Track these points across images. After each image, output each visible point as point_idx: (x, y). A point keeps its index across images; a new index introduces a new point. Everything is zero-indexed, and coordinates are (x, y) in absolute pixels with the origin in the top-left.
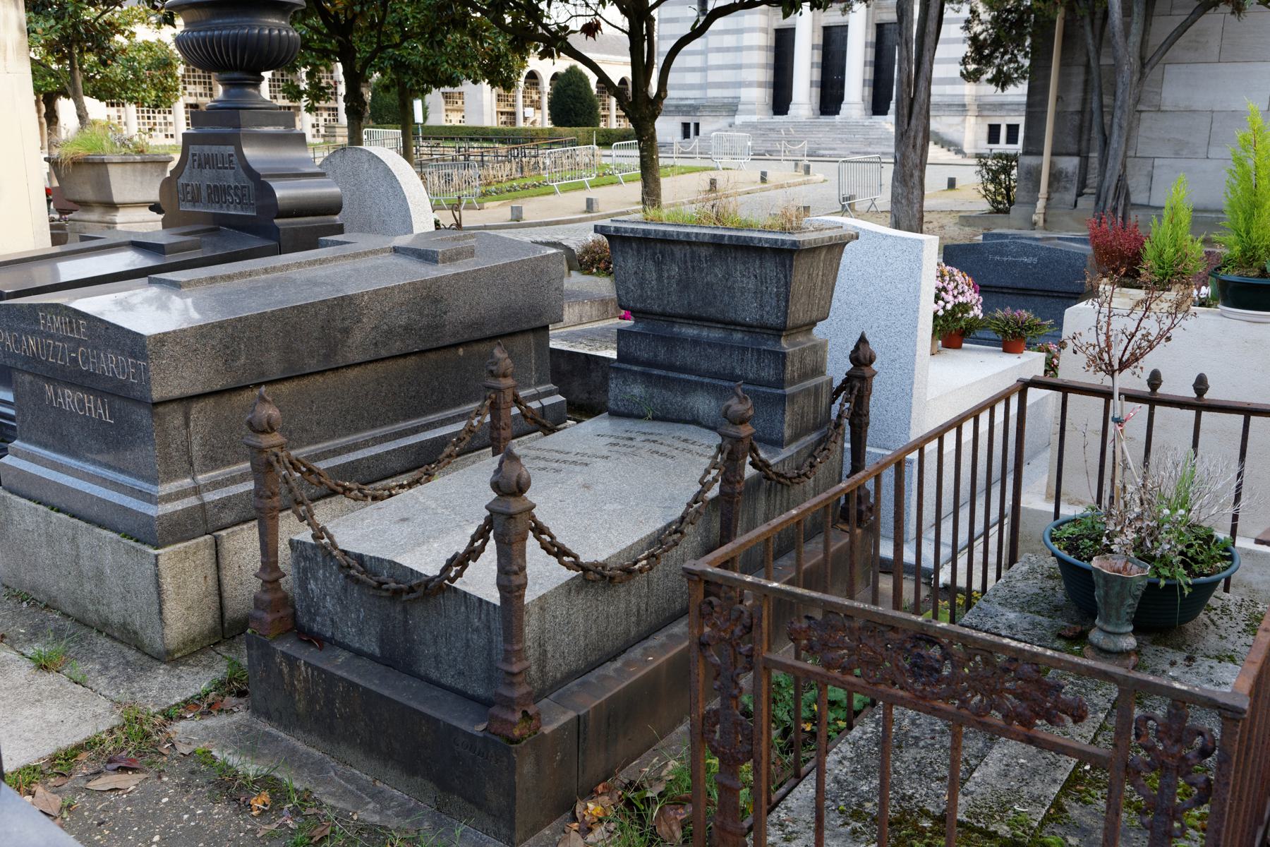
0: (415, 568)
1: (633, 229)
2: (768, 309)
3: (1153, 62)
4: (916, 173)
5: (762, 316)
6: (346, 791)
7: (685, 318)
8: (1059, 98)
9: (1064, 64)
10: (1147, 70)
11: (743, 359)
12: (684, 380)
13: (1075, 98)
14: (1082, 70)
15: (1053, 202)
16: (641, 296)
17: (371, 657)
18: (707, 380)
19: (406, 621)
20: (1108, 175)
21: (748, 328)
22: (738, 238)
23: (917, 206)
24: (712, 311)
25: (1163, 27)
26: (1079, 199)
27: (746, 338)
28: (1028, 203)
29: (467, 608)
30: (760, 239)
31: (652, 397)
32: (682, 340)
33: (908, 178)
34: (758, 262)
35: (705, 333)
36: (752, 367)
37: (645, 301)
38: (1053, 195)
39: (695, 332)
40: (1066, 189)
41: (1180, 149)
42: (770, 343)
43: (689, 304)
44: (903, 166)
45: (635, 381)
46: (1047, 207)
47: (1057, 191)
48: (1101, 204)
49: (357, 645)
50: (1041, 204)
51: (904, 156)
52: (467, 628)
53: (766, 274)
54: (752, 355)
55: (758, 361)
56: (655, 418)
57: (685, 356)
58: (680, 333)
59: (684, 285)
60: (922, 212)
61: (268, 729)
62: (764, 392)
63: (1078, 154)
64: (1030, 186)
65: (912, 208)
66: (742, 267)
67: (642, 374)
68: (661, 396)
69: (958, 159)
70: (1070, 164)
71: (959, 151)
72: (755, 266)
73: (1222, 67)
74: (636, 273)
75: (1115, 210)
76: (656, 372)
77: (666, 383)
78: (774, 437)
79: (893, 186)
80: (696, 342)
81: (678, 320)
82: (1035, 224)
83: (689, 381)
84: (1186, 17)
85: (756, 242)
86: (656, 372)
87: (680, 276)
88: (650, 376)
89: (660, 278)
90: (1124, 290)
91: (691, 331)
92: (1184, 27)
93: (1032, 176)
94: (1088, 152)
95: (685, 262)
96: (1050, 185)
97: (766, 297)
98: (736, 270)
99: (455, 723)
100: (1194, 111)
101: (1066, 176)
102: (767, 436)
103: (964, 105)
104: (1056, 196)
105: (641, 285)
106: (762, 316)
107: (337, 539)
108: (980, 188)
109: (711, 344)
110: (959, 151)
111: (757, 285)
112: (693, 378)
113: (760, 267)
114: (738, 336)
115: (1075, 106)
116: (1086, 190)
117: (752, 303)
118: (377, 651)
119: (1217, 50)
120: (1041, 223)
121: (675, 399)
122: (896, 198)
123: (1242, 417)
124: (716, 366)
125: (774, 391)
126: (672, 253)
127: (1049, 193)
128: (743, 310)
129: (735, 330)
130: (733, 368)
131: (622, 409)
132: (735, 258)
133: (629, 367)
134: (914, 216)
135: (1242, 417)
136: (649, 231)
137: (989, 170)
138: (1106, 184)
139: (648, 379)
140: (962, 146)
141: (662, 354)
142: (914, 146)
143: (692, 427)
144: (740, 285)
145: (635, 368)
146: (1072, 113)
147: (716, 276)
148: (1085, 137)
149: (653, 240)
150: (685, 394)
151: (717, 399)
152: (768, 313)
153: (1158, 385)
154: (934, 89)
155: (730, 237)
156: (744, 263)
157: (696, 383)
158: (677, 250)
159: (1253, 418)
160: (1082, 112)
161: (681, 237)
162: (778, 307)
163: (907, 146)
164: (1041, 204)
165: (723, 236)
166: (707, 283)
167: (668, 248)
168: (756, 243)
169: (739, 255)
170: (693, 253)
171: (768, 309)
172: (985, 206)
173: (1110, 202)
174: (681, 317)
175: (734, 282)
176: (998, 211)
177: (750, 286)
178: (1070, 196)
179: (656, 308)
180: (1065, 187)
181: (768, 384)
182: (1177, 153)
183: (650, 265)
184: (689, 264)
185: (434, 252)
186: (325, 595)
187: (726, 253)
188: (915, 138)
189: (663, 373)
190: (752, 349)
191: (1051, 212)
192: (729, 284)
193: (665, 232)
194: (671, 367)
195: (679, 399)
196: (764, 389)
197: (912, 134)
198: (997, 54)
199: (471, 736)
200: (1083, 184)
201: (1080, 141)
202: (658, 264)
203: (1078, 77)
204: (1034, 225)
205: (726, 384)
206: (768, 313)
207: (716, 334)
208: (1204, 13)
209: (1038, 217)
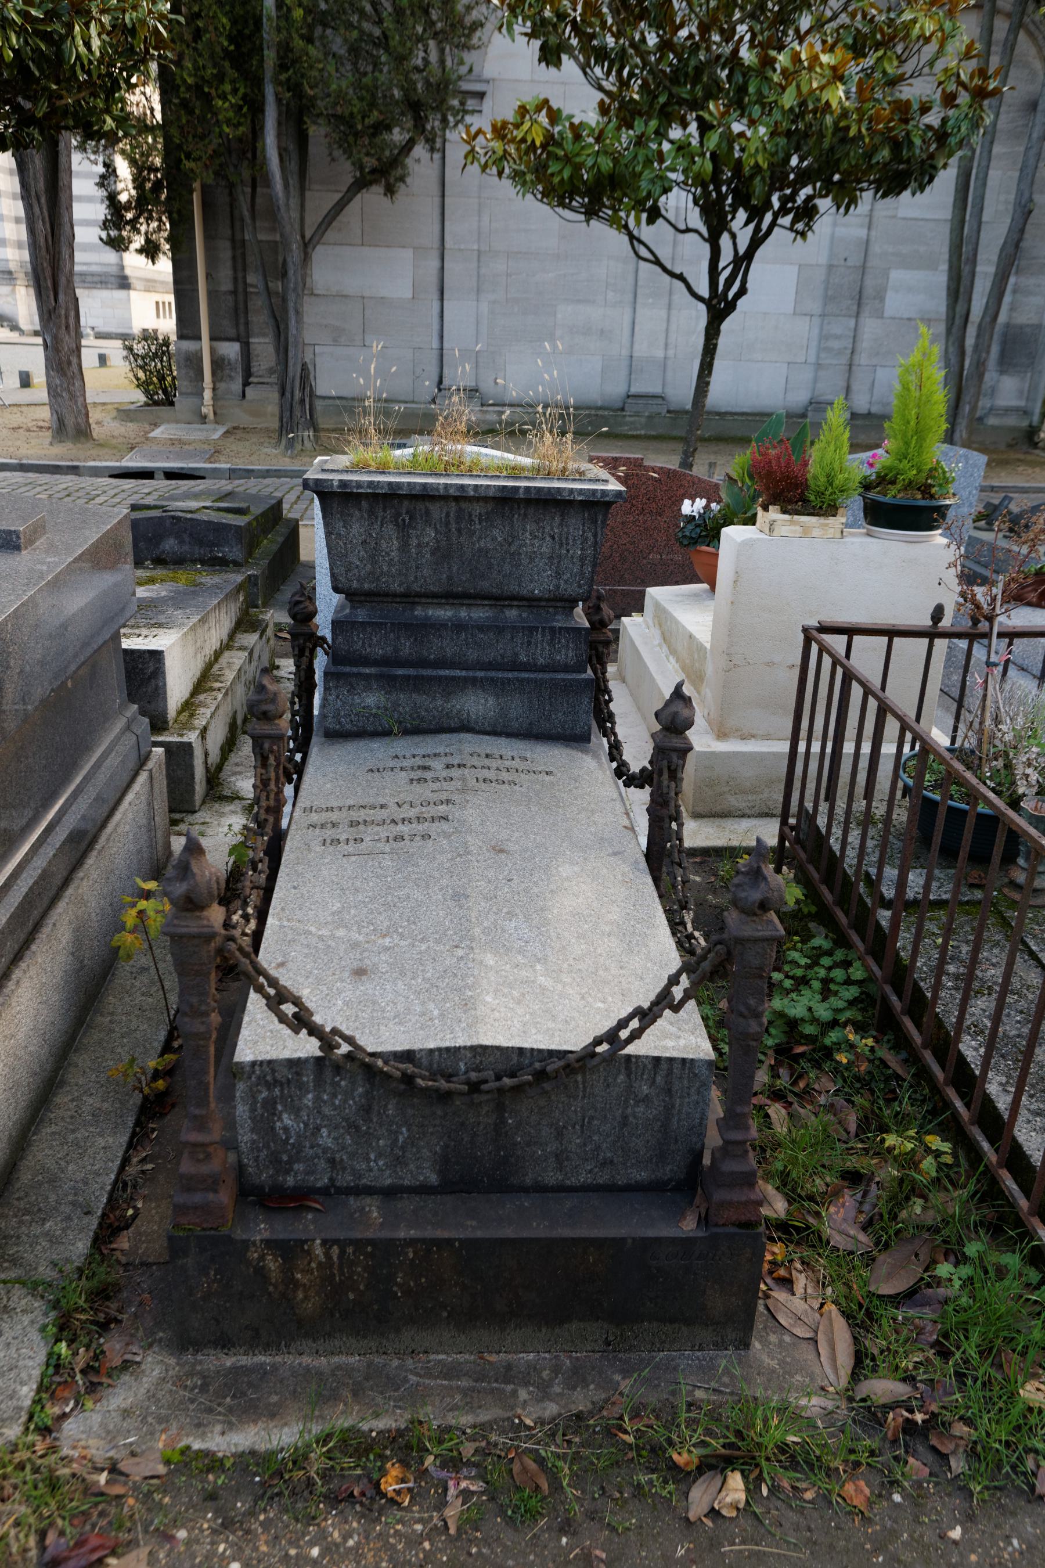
0: (526, 1045)
1: (371, 482)
2: (567, 576)
3: (314, 241)
4: (74, 360)
5: (558, 587)
6: (465, 1392)
7: (428, 597)
8: (208, 276)
9: (208, 237)
10: (309, 250)
11: (529, 643)
12: (446, 677)
13: (225, 273)
14: (228, 244)
15: (219, 392)
16: (372, 573)
17: (423, 1190)
18: (480, 674)
19: (503, 1121)
20: (291, 364)
21: (530, 602)
22: (539, 489)
23: (81, 399)
24: (484, 585)
25: (320, 201)
26: (247, 389)
27: (524, 615)
28: (192, 394)
29: (629, 1076)
30: (571, 491)
31: (396, 705)
32: (438, 627)
33: (65, 366)
34: (557, 519)
35: (463, 613)
36: (543, 649)
37: (378, 579)
38: (218, 385)
39: (449, 613)
40: (231, 378)
41: (338, 335)
42: (558, 617)
43: (450, 578)
44: (57, 351)
45: (368, 688)
46: (215, 398)
47: (221, 380)
48: (288, 395)
49: (389, 1181)
50: (208, 394)
51: (56, 338)
52: (626, 1101)
53: (568, 533)
54: (543, 636)
55: (551, 643)
56: (407, 732)
57: (445, 646)
58: (427, 618)
59: (442, 554)
60: (86, 406)
61: (229, 1362)
62: (564, 680)
63: (237, 339)
64: (192, 374)
65: (76, 402)
66: (534, 526)
67: (379, 677)
68: (407, 702)
69: (14, 336)
70: (231, 350)
71: (15, 327)
72: (553, 524)
73: (366, 250)
74: (364, 542)
75: (302, 401)
76: (400, 672)
77: (418, 684)
78: (578, 731)
79: (48, 375)
80: (459, 627)
81: (423, 600)
82: (205, 417)
83: (453, 678)
84: (340, 195)
85: (565, 494)
86: (400, 672)
87: (438, 542)
88: (394, 678)
89: (404, 547)
90: (796, 517)
91: (443, 613)
92: (340, 207)
93: (193, 362)
94: (248, 337)
95: (447, 524)
96: (214, 374)
97: (565, 563)
98: (525, 530)
99: (651, 1233)
100: (346, 296)
101: (229, 364)
102: (569, 732)
103: (10, 273)
104: (222, 386)
105: (373, 558)
106: (558, 587)
107: (361, 1041)
108: (131, 375)
109: (481, 628)
110: (15, 327)
111: (553, 548)
112: (458, 673)
113: (561, 525)
114: (512, 614)
115: (226, 286)
116: (251, 379)
117: (545, 571)
118: (433, 1179)
119: (359, 232)
120: (211, 416)
121: (431, 704)
122: (55, 391)
123: (886, 639)
124: (490, 655)
125: (574, 676)
126: (427, 512)
127: (214, 382)
128: (531, 581)
129: (504, 606)
130: (516, 654)
131: (348, 727)
132: (525, 515)
133: (355, 670)
134: (79, 411)
135: (886, 639)
136: (399, 485)
137: (136, 356)
138: (291, 374)
139: (390, 683)
140: (17, 322)
141: (407, 647)
142: (67, 327)
143: (464, 736)
144: (530, 549)
145: (367, 671)
146: (225, 293)
147: (494, 539)
148: (242, 321)
149: (405, 496)
150: (447, 695)
151: (497, 696)
152: (566, 582)
153: (940, 620)
154: (78, 257)
155: (528, 488)
156: (537, 522)
157: (465, 679)
158: (437, 511)
159: (896, 640)
160: (234, 292)
161: (452, 492)
162: (582, 573)
163: (59, 327)
164: (208, 394)
165: (517, 488)
166: (480, 550)
167: (420, 506)
168: (482, 493)
169: (531, 511)
170: (460, 510)
171: (567, 576)
172: (140, 397)
173: (298, 394)
174: (435, 596)
175: (521, 546)
176: (156, 403)
177: (544, 549)
178: (237, 386)
179: (396, 587)
180: (230, 376)
181: (566, 669)
182: (335, 340)
183: (390, 530)
184: (453, 526)
185: (10, 532)
186: (318, 1128)
187: (512, 509)
188: (67, 317)
189: (412, 672)
190: (544, 629)
191: (219, 403)
192: (513, 549)
193: (425, 485)
194: (423, 663)
195: (439, 702)
196: (561, 676)
197: (63, 312)
198: (142, 220)
199: (686, 1243)
200: (247, 373)
201: (237, 325)
202: (404, 529)
203: (225, 254)
204: (203, 419)
205: (510, 675)
206: (566, 582)
207: (480, 614)
208: (359, 191)
209: (207, 410)
